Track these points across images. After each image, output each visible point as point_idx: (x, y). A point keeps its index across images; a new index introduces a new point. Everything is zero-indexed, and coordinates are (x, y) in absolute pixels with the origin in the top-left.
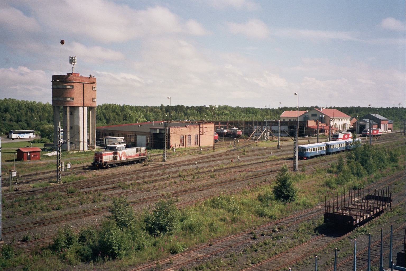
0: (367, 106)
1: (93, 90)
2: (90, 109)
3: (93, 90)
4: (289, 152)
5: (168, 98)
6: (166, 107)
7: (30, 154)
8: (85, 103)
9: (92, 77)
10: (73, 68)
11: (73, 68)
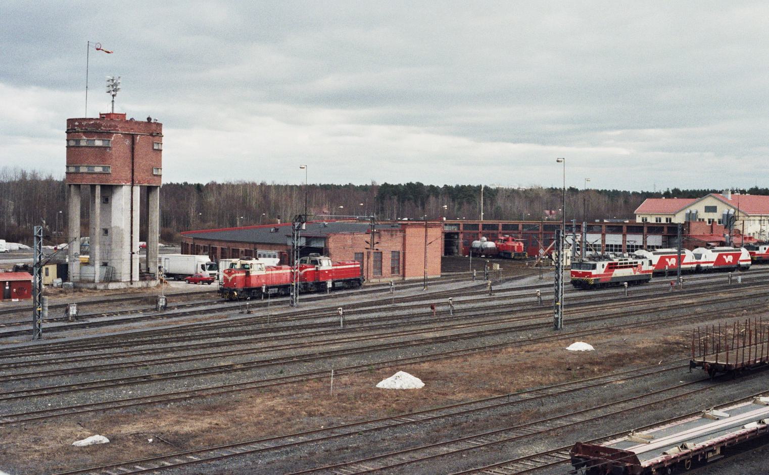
0: (369, 184)
1: (153, 149)
2: (148, 191)
3: (153, 149)
4: (548, 290)
5: (558, 161)
6: (381, 187)
7: (10, 286)
8: (135, 178)
9: (152, 121)
10: (113, 101)
11: (113, 101)
